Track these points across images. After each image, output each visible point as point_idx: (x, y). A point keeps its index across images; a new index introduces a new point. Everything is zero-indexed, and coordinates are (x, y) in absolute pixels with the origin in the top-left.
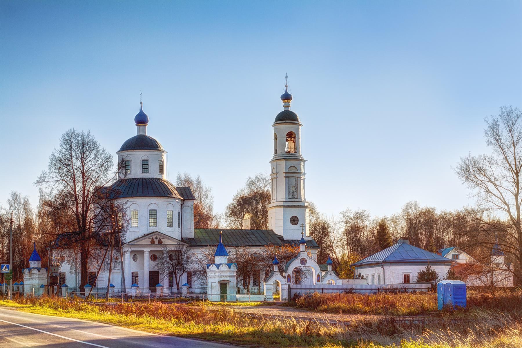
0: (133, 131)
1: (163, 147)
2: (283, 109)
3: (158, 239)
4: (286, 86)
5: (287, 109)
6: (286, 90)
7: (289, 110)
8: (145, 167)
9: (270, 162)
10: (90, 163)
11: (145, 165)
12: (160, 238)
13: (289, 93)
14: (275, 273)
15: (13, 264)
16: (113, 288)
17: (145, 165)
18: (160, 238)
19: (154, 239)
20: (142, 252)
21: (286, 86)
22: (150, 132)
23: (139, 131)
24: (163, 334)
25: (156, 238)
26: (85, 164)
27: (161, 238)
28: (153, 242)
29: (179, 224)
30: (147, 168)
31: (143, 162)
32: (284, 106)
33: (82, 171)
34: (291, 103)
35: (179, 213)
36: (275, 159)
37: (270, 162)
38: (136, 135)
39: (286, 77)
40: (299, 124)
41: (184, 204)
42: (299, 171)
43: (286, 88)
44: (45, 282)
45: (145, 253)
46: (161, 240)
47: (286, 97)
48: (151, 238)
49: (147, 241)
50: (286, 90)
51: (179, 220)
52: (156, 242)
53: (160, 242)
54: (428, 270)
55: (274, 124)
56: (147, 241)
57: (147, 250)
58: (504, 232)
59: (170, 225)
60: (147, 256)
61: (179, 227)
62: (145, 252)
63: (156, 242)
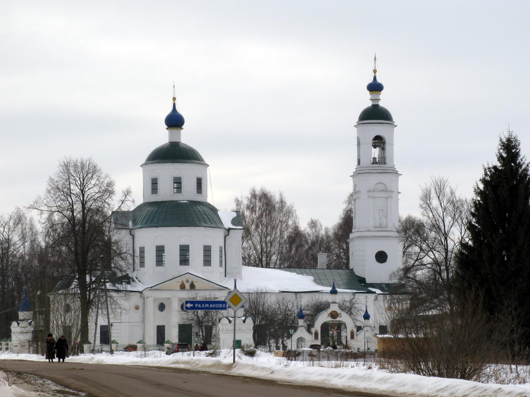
1: (207, 160)
2: (369, 104)
3: (189, 283)
4: (375, 71)
5: (375, 103)
6: (375, 78)
7: (379, 105)
9: (351, 176)
10: (91, 190)
13: (379, 80)
14: (299, 328)
16: (116, 345)
21: (375, 71)
23: (171, 136)
24: (21, 392)
26: (85, 192)
28: (183, 287)
29: (221, 262)
30: (180, 187)
32: (371, 100)
33: (81, 201)
35: (221, 248)
36: (357, 172)
37: (351, 176)
39: (375, 59)
40: (393, 124)
41: (228, 235)
43: (375, 74)
44: (29, 337)
46: (193, 283)
49: (176, 284)
50: (375, 78)
51: (221, 257)
52: (187, 286)
53: (192, 286)
54: (39, 346)
55: (357, 124)
59: (207, 262)
61: (221, 265)
63: (187, 286)
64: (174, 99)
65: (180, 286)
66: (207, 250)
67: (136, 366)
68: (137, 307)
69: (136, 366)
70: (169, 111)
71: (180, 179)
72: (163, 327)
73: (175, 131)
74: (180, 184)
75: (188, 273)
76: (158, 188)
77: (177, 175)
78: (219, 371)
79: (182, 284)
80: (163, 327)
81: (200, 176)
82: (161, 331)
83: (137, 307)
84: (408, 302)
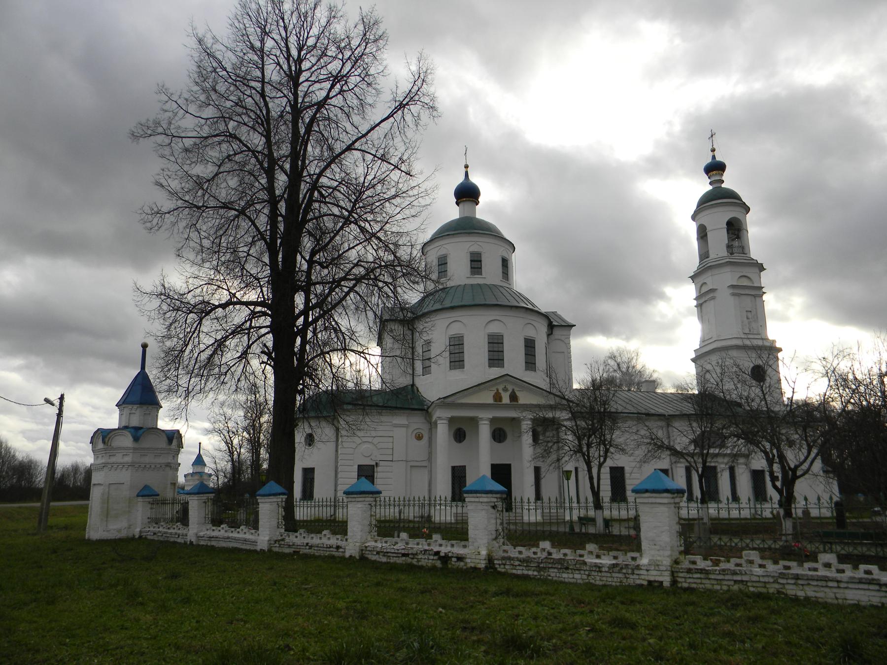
0: (453, 212)
4: (713, 150)
6: (714, 157)
8: (476, 265)
9: (695, 299)
11: (476, 264)
12: (513, 390)
15: (257, 514)
17: (476, 264)
18: (513, 390)
19: (501, 391)
20: (474, 422)
22: (482, 212)
25: (505, 390)
27: (516, 389)
28: (498, 397)
30: (480, 266)
31: (471, 257)
34: (726, 176)
38: (458, 217)
41: (552, 334)
42: (756, 285)
45: (481, 422)
47: (715, 168)
48: (495, 389)
49: (487, 398)
50: (714, 157)
52: (506, 400)
53: (514, 397)
56: (487, 398)
57: (485, 416)
58: (761, 546)
59: (530, 364)
60: (485, 431)
62: (482, 419)
64: (466, 167)
65: (494, 396)
66: (530, 345)
67: (738, 522)
68: (419, 435)
69: (738, 522)
70: (461, 179)
71: (479, 254)
72: (463, 468)
73: (467, 205)
74: (480, 263)
75: (507, 375)
76: (448, 270)
77: (475, 248)
78: (46, 497)
79: (496, 393)
80: (463, 468)
81: (506, 255)
82: (458, 475)
83: (419, 435)
84: (784, 431)
